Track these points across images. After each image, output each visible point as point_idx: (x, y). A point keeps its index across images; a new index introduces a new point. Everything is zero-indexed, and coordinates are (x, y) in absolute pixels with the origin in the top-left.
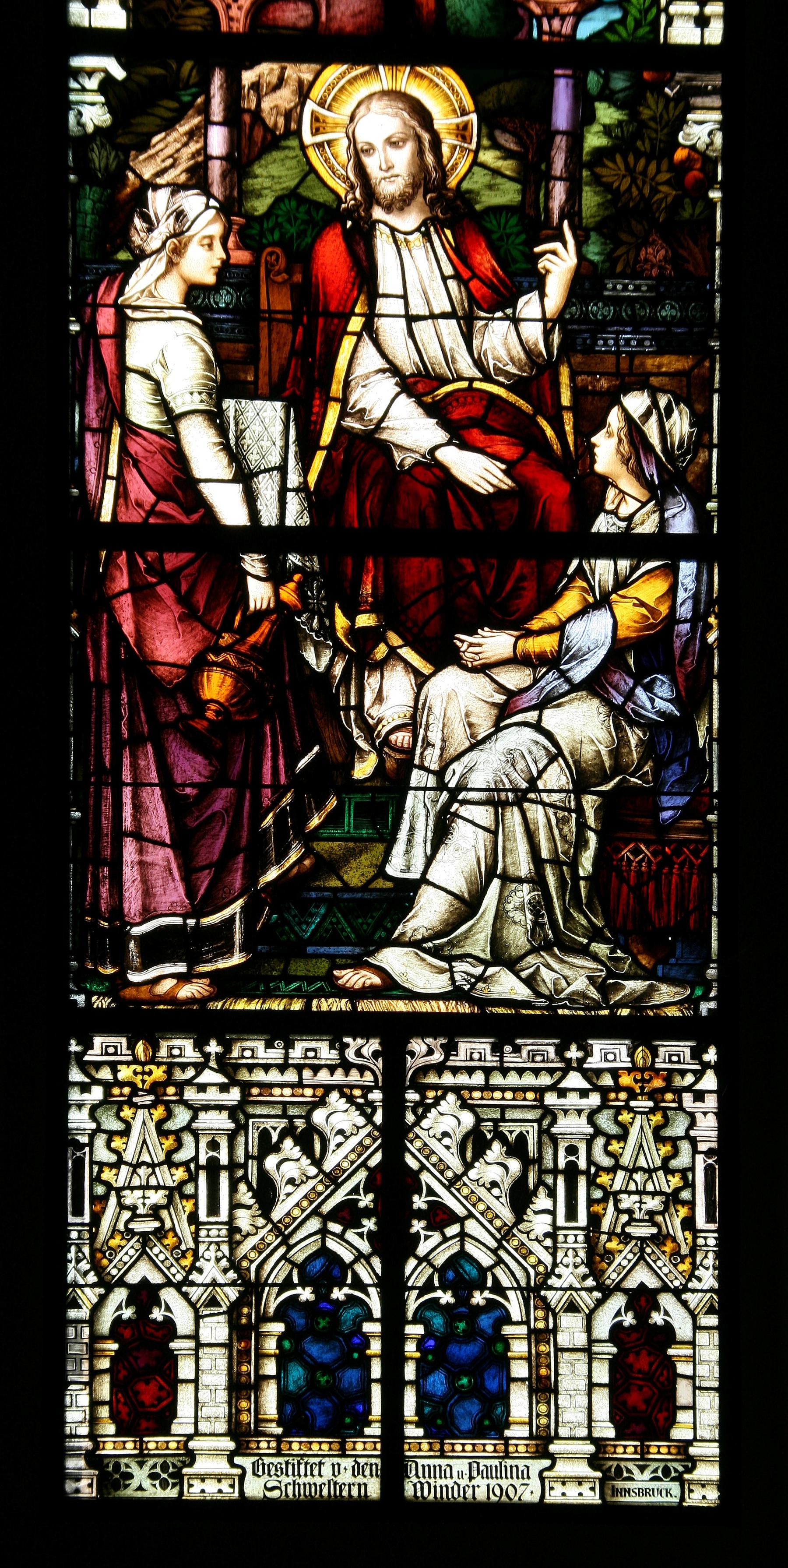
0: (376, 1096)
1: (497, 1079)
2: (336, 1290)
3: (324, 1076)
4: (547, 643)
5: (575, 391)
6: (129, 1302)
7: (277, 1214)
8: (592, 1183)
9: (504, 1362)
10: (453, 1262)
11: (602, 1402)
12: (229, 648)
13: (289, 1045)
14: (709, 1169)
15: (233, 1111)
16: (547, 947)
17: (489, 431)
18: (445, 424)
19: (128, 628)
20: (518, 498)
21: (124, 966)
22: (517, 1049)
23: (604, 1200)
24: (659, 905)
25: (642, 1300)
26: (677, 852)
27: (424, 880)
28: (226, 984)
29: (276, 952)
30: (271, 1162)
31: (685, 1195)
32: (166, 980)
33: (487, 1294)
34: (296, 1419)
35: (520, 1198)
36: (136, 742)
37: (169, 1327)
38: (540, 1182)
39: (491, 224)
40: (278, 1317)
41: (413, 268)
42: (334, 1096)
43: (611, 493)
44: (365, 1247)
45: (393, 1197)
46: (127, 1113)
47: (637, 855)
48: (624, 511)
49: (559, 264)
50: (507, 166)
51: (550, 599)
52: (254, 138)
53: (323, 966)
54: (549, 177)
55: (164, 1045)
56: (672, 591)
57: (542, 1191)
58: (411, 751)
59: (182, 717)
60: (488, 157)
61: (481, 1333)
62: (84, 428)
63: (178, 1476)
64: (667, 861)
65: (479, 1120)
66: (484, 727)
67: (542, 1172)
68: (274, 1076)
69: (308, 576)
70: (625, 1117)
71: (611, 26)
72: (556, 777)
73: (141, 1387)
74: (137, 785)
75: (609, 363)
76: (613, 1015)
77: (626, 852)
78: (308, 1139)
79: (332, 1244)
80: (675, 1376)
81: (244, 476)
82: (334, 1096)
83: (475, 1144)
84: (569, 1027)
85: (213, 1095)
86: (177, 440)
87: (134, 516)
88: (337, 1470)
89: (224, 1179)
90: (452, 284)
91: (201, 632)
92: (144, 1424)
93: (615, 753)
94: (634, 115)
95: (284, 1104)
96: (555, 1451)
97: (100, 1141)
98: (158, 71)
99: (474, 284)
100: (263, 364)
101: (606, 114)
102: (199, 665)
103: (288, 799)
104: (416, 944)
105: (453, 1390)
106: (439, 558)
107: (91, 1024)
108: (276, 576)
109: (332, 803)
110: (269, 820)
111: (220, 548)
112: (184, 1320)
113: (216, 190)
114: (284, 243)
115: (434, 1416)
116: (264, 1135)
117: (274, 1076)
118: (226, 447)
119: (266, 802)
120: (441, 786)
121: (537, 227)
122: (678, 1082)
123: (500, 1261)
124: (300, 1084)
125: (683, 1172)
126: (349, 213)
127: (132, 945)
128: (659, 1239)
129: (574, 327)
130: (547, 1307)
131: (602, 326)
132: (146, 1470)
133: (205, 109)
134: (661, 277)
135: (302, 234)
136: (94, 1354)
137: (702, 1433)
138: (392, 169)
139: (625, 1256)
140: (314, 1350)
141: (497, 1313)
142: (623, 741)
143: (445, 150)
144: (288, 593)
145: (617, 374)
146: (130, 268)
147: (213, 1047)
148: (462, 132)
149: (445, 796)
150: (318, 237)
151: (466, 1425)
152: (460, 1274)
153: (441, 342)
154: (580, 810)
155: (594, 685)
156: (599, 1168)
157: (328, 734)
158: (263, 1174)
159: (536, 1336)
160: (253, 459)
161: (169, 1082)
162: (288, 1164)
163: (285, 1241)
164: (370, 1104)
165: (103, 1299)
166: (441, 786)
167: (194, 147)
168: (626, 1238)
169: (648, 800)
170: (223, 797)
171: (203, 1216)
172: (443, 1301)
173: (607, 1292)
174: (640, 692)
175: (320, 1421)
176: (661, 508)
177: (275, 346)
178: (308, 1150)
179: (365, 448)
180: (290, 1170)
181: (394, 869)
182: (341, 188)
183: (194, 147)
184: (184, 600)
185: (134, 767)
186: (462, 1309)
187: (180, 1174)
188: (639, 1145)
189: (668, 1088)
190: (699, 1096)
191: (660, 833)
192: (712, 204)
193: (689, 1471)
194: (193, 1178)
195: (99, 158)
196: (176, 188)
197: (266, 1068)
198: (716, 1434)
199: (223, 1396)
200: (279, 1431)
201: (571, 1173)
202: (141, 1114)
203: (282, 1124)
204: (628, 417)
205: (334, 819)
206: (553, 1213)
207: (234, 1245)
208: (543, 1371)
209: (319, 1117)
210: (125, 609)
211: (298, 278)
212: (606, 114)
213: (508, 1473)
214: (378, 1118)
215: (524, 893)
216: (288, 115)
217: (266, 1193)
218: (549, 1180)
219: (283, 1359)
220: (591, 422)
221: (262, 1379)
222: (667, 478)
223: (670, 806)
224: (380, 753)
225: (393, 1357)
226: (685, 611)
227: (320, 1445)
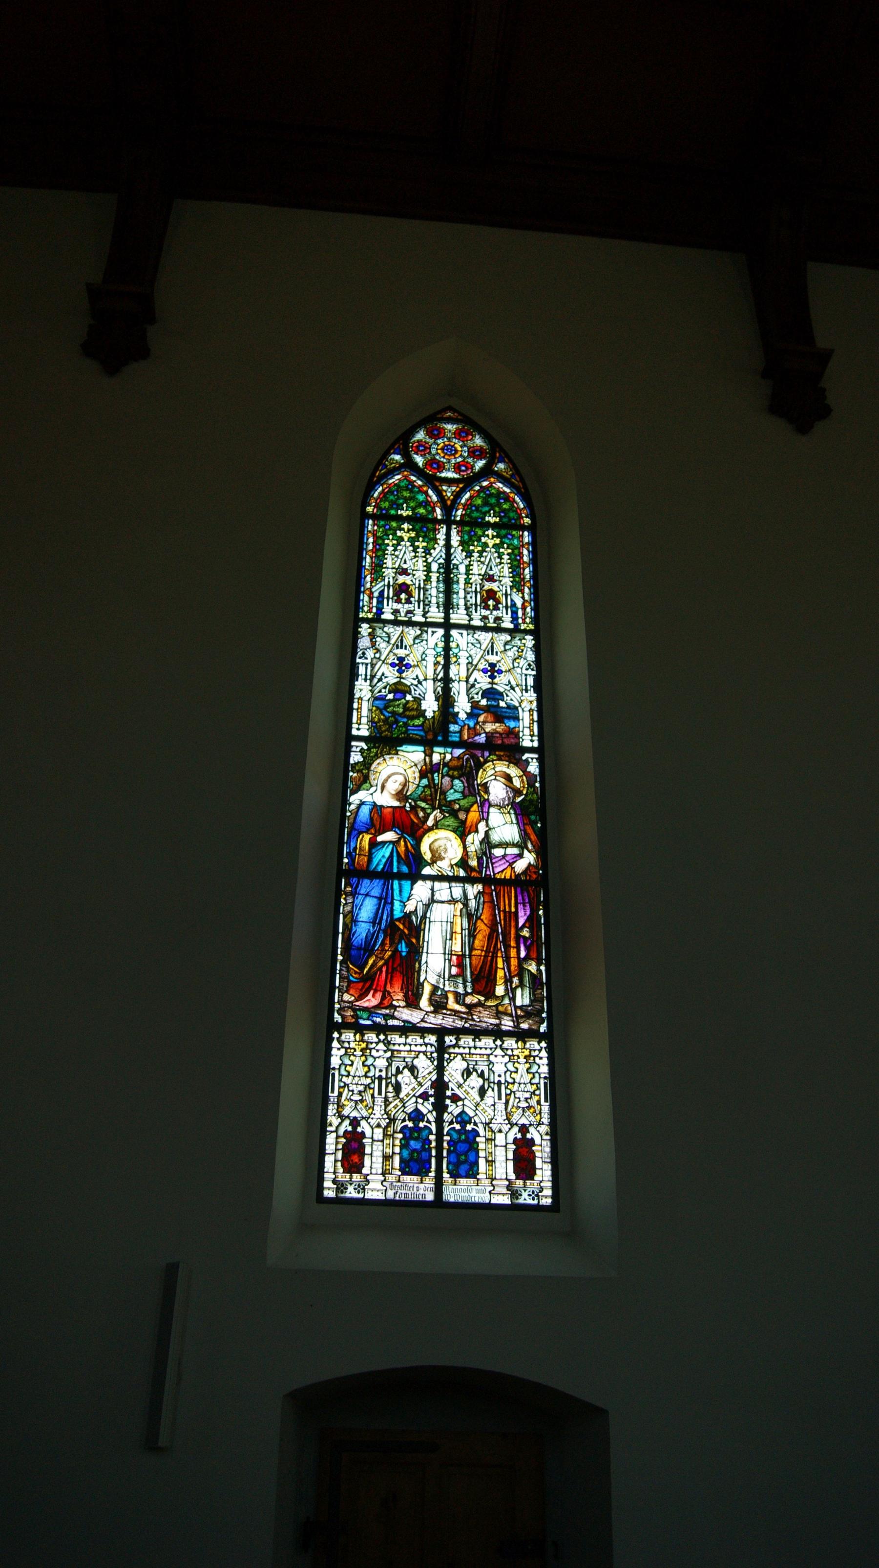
0: (435, 1055)
1: (473, 1051)
7: (401, 1096)
8: (506, 1088)
11: (511, 1165)
13: (407, 1037)
14: (545, 1084)
22: (480, 1040)
23: (344, 1087)
25: (524, 1129)
30: (400, 1077)
31: (537, 1092)
33: (425, 1123)
35: (482, 1092)
37: (363, 1135)
38: (489, 1086)
40: (401, 1132)
42: (421, 1054)
44: (431, 1108)
57: (490, 1089)
63: (364, 1189)
65: (468, 1065)
67: (489, 1083)
68: (402, 1048)
78: (412, 1069)
79: (420, 1107)
80: (534, 1157)
82: (421, 1054)
83: (467, 1073)
85: (381, 1053)
89: (384, 1082)
95: (405, 1058)
96: (490, 1183)
112: (368, 1133)
116: (398, 1068)
124: (411, 1051)
125: (537, 1084)
130: (493, 1131)
132: (527, 1193)
152: (463, 1119)
156: (509, 1083)
158: (397, 1082)
162: (405, 1077)
165: (340, 1124)
171: (376, 1095)
178: (413, 1074)
180: (407, 1080)
186: (463, 1130)
190: (541, 1058)
193: (541, 1192)
194: (373, 1082)
197: (399, 1045)
198: (550, 1179)
199: (381, 1159)
200: (400, 1173)
214: (436, 1063)
217: (398, 1088)
218: (492, 1085)
225: (439, 1148)
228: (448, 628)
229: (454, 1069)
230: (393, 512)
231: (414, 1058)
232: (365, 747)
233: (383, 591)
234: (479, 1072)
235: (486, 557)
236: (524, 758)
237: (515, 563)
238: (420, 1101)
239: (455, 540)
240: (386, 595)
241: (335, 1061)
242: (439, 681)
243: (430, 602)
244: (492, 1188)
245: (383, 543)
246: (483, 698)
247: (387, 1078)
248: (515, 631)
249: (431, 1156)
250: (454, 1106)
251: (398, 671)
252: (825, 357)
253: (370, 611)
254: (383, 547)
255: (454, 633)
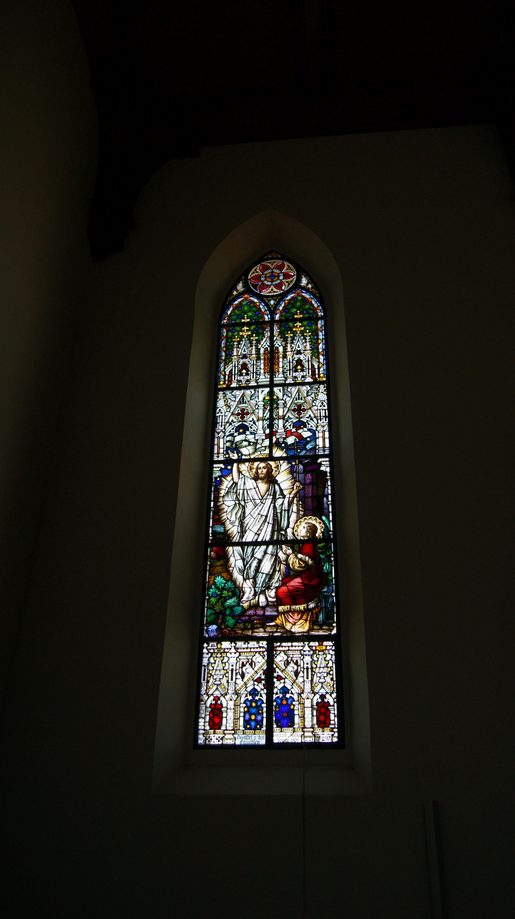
0: (266, 653)
1: (291, 648)
2: (287, 694)
6: (214, 700)
10: (282, 688)
13: (248, 643)
30: (244, 668)
31: (331, 673)
35: (297, 674)
44: (263, 688)
45: (269, 675)
70: (215, 659)
79: (256, 687)
83: (287, 663)
85: (307, 653)
112: (225, 705)
116: (243, 663)
125: (331, 667)
137: (229, 728)
152: (285, 690)
164: (264, 655)
171: (230, 681)
172: (249, 699)
197: (244, 648)
203: (247, 661)
206: (303, 677)
214: (266, 658)
229: (280, 659)
230: (238, 321)
231: (253, 656)
232: (223, 467)
233: (232, 369)
234: (295, 661)
235: (302, 340)
236: (319, 461)
237: (314, 341)
238: (256, 683)
239: (276, 333)
240: (233, 373)
241: (205, 661)
242: (266, 420)
243: (260, 373)
244: (302, 733)
245: (232, 341)
246: (236, 432)
247: (236, 670)
248: (316, 382)
249: (263, 718)
250: (279, 682)
251: (241, 418)
253: (224, 383)
254: (231, 344)
255: (276, 389)
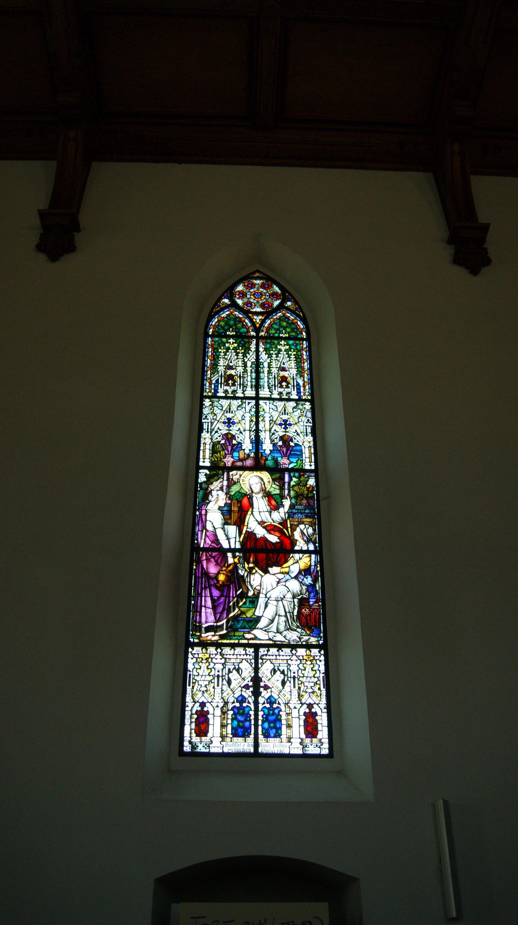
3: (242, 657)
4: (287, 570)
5: (291, 525)
7: (232, 687)
8: (298, 680)
9: (280, 720)
10: (269, 698)
12: (225, 570)
15: (223, 664)
16: (288, 629)
17: (274, 531)
18: (266, 530)
19: (205, 567)
20: (281, 544)
21: (200, 631)
23: (301, 683)
24: (310, 621)
25: (310, 706)
26: (314, 610)
27: (263, 616)
28: (222, 637)
29: (232, 629)
30: (230, 675)
32: (210, 636)
34: (235, 734)
35: (283, 683)
36: (206, 588)
38: (288, 680)
39: (274, 496)
41: (260, 504)
42: (244, 660)
43: (298, 542)
44: (251, 694)
46: (200, 664)
47: (305, 611)
48: (301, 546)
49: (287, 503)
50: (277, 487)
51: (286, 561)
52: (231, 483)
53: (242, 633)
54: (284, 489)
55: (209, 650)
56: (310, 560)
57: (288, 682)
58: (260, 590)
59: (215, 584)
60: (274, 486)
61: (276, 714)
62: (198, 530)
64: (312, 612)
65: (274, 666)
66: (275, 586)
67: (288, 677)
68: (231, 657)
69: (240, 557)
70: (305, 665)
71: (295, 466)
72: (289, 596)
73: (201, 726)
74: (205, 596)
75: (297, 520)
76: (302, 644)
77: (303, 610)
81: (228, 539)
82: (244, 660)
83: (274, 671)
84: (293, 647)
86: (216, 533)
87: (207, 546)
88: (244, 746)
89: (220, 678)
90: (268, 506)
91: (219, 567)
92: (202, 734)
93: (301, 591)
94: (299, 480)
96: (290, 741)
97: (195, 670)
98: (215, 472)
99: (271, 506)
100: (232, 519)
101: (294, 479)
102: (219, 573)
103: (235, 599)
104: (261, 629)
105: (269, 727)
106: (267, 554)
107: (193, 645)
108: (234, 557)
109: (244, 600)
110: (231, 604)
111: (223, 552)
113: (225, 491)
114: (237, 500)
115: (265, 733)
117: (231, 657)
118: (225, 534)
119: (231, 600)
120: (266, 597)
121: (282, 497)
122: (316, 658)
123: (279, 697)
125: (318, 677)
126: (249, 495)
127: (203, 629)
128: (313, 692)
129: (290, 514)
131: (295, 513)
132: (202, 745)
133: (223, 478)
134: (306, 506)
135: (240, 498)
136: (191, 718)
138: (256, 488)
139: (306, 696)
140: (239, 717)
141: (279, 709)
142: (302, 588)
143: (266, 485)
144: (236, 560)
145: (298, 522)
146: (208, 503)
147: (219, 650)
148: (269, 482)
149: (267, 599)
150: (243, 498)
151: (272, 735)
152: (271, 701)
153: (266, 517)
154: (294, 602)
155: (296, 577)
157: (243, 587)
159: (288, 714)
160: (230, 536)
161: (209, 657)
162: (234, 675)
163: (233, 693)
165: (194, 705)
166: (266, 597)
167: (221, 484)
168: (306, 692)
169: (307, 600)
170: (223, 599)
173: (302, 704)
174: (305, 579)
175: (240, 734)
176: (308, 545)
177: (235, 516)
178: (238, 673)
179: (251, 535)
181: (257, 614)
182: (247, 491)
183: (221, 484)
184: (216, 561)
185: (205, 593)
187: (211, 678)
188: (308, 672)
189: (314, 659)
190: (320, 661)
191: (310, 606)
192: (314, 494)
193: (321, 745)
194: (214, 678)
195: (204, 486)
196: (217, 490)
198: (327, 737)
200: (231, 736)
201: (294, 678)
202: (204, 664)
204: (301, 530)
205: (245, 603)
207: (222, 693)
208: (289, 723)
209: (241, 665)
210: (205, 563)
211: (239, 505)
212: (294, 479)
213: (282, 746)
215: (283, 619)
216: (238, 479)
217: (229, 682)
218: (289, 679)
219: (232, 720)
220: (293, 529)
221: (227, 724)
222: (308, 541)
223: (312, 601)
224: (254, 590)
226: (313, 564)
227: (241, 739)
228: (261, 407)
252: (485, 228)
